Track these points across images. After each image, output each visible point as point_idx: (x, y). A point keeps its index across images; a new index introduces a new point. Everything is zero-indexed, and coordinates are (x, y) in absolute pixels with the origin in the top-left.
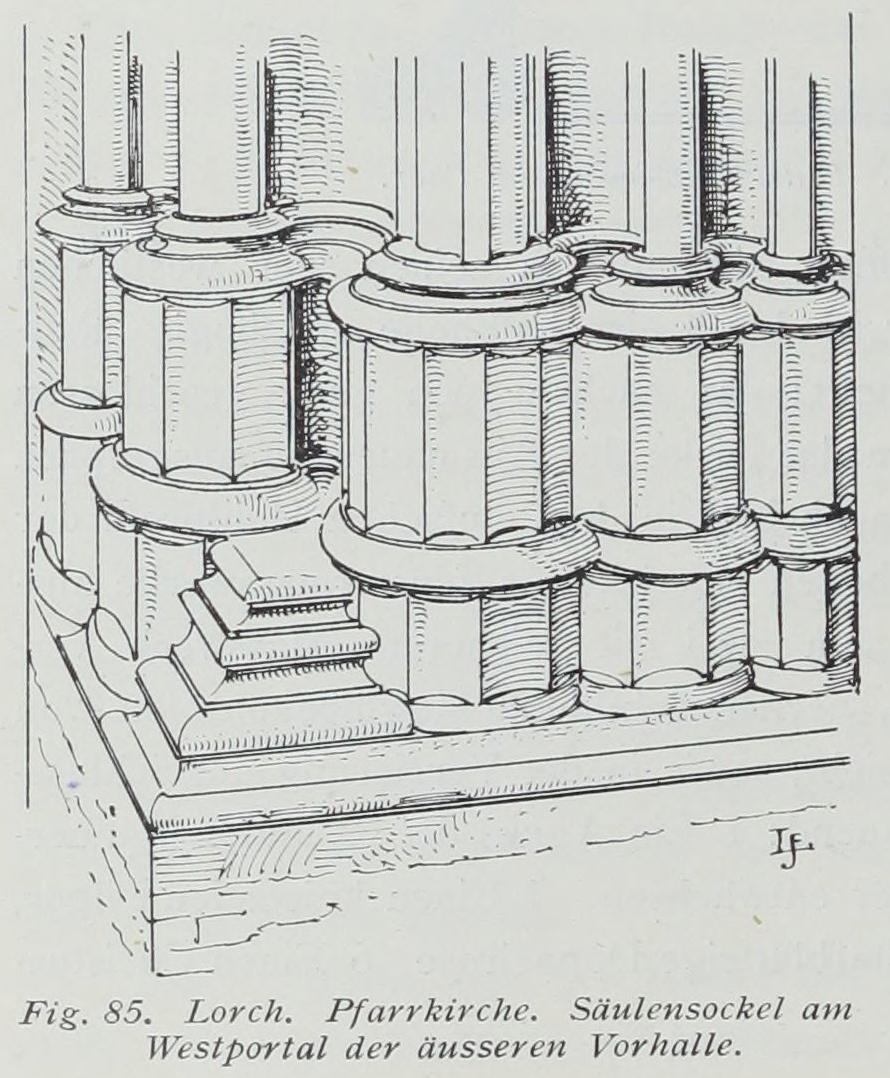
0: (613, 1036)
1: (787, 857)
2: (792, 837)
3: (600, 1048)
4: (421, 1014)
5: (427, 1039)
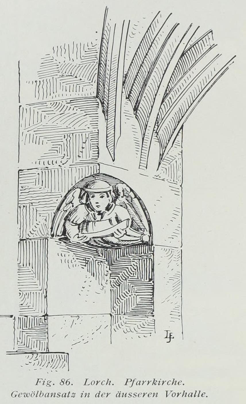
0: (171, 391)
1: (168, 340)
2: (170, 334)
3: (168, 395)
4: (151, 383)
5: (32, 392)
